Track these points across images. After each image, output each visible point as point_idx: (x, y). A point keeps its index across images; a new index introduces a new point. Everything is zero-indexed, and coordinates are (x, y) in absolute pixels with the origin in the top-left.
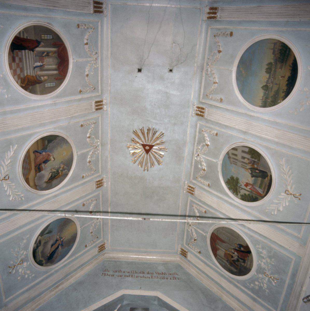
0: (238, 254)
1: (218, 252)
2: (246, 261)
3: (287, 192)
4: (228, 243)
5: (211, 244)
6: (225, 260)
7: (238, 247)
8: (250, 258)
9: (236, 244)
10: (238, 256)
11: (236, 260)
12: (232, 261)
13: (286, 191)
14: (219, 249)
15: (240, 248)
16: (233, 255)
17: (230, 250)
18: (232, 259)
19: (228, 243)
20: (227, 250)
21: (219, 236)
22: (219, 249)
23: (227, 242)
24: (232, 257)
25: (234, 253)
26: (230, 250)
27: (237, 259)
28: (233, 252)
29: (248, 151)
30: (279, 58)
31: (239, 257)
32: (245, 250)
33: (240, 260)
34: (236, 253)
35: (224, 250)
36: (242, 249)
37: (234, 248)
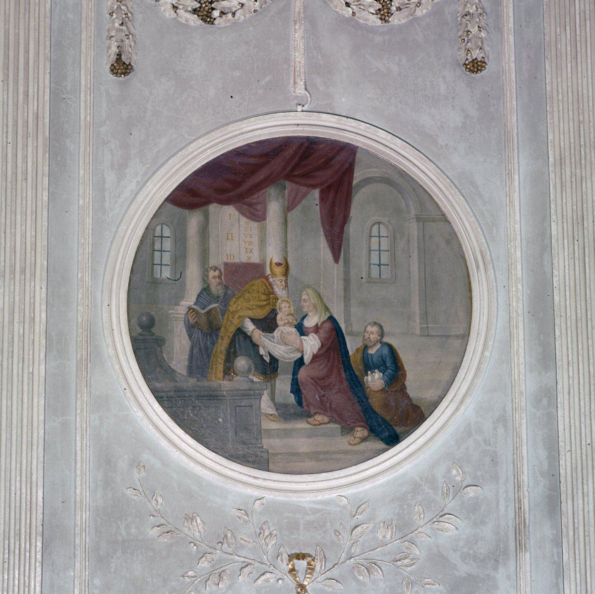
0: (315, 357)
1: (230, 211)
2: (301, 425)
3: (301, 564)
4: (347, 272)
5: (237, 153)
6: (205, 278)
7: (366, 347)
8: (343, 442)
9: (382, 335)
10: (300, 362)
11: (262, 352)
12: (233, 329)
13: (300, 556)
14: (257, 215)
15: (369, 366)
16: (285, 329)
17: (308, 296)
18: (250, 327)
19: (347, 272)
20: (286, 273)
21: (358, 199)
22: (257, 215)
23: (347, 262)
24: (268, 324)
25: (302, 330)
26: (308, 296)
27: (274, 360)
28: (309, 323)
29: (239, 358)
30: (342, 427)
31: (303, 374)
32: (375, 402)
33: (283, 384)
34: (311, 345)
35: (273, 254)
36: (375, 380)
37: (343, 326)
